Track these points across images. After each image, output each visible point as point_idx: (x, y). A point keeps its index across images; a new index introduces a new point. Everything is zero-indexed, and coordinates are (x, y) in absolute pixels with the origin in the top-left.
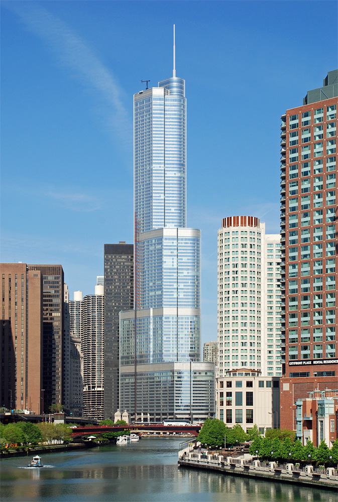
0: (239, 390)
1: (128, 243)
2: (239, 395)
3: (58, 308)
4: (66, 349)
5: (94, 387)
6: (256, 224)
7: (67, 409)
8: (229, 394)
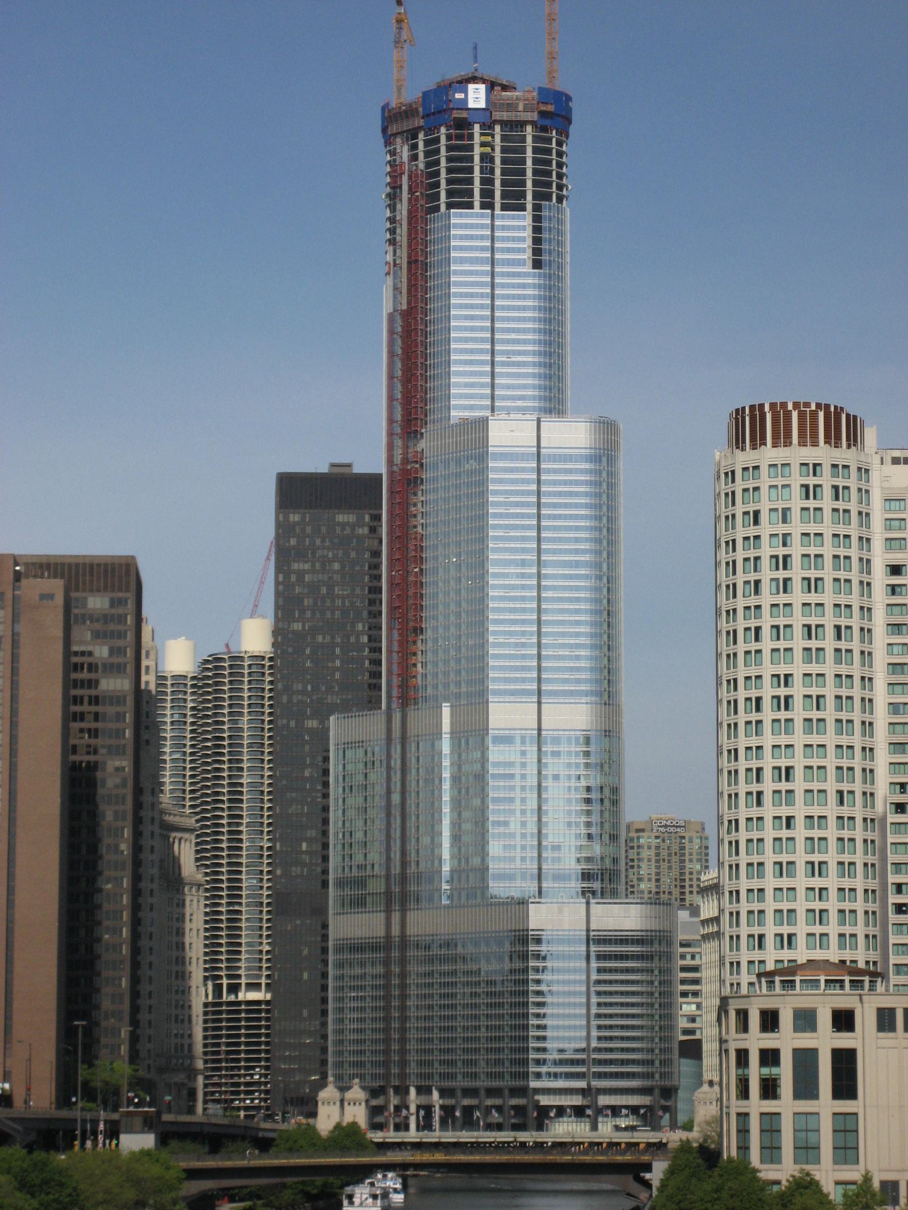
0: (805, 1041)
1: (359, 468)
2: (805, 1060)
3: (120, 709)
4: (146, 856)
5: (234, 989)
6: (854, 439)
7: (148, 1076)
8: (770, 1057)
